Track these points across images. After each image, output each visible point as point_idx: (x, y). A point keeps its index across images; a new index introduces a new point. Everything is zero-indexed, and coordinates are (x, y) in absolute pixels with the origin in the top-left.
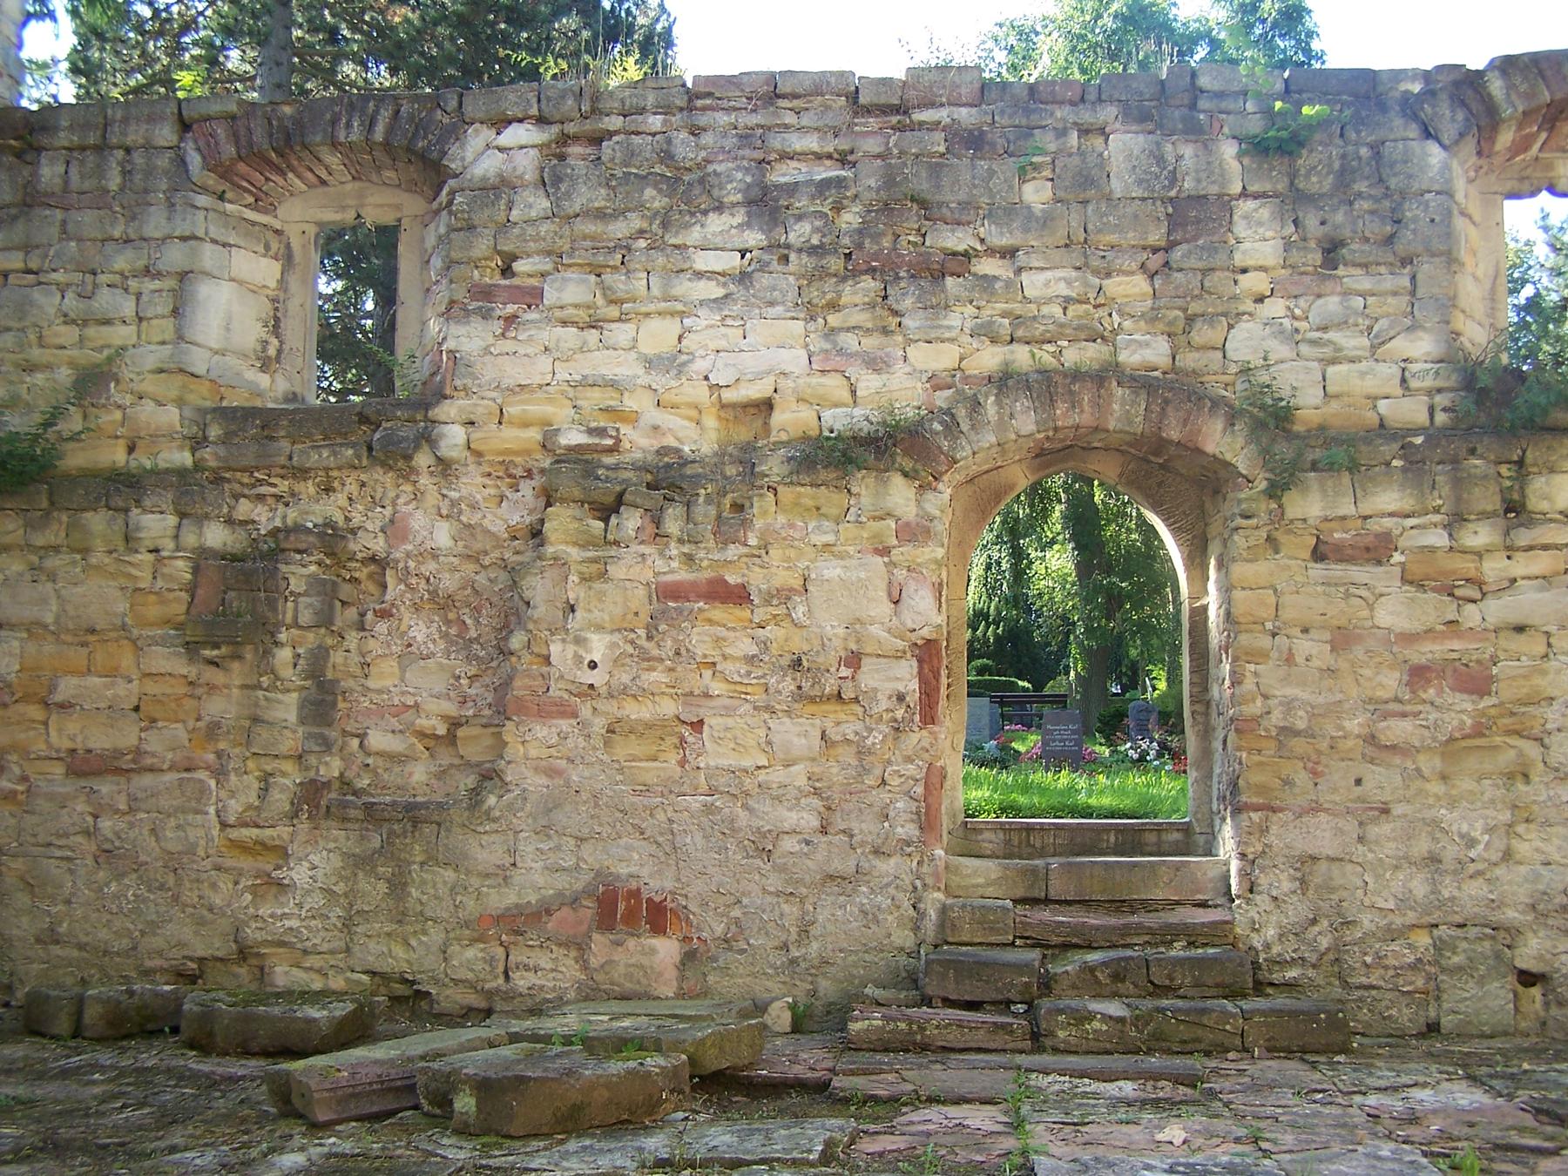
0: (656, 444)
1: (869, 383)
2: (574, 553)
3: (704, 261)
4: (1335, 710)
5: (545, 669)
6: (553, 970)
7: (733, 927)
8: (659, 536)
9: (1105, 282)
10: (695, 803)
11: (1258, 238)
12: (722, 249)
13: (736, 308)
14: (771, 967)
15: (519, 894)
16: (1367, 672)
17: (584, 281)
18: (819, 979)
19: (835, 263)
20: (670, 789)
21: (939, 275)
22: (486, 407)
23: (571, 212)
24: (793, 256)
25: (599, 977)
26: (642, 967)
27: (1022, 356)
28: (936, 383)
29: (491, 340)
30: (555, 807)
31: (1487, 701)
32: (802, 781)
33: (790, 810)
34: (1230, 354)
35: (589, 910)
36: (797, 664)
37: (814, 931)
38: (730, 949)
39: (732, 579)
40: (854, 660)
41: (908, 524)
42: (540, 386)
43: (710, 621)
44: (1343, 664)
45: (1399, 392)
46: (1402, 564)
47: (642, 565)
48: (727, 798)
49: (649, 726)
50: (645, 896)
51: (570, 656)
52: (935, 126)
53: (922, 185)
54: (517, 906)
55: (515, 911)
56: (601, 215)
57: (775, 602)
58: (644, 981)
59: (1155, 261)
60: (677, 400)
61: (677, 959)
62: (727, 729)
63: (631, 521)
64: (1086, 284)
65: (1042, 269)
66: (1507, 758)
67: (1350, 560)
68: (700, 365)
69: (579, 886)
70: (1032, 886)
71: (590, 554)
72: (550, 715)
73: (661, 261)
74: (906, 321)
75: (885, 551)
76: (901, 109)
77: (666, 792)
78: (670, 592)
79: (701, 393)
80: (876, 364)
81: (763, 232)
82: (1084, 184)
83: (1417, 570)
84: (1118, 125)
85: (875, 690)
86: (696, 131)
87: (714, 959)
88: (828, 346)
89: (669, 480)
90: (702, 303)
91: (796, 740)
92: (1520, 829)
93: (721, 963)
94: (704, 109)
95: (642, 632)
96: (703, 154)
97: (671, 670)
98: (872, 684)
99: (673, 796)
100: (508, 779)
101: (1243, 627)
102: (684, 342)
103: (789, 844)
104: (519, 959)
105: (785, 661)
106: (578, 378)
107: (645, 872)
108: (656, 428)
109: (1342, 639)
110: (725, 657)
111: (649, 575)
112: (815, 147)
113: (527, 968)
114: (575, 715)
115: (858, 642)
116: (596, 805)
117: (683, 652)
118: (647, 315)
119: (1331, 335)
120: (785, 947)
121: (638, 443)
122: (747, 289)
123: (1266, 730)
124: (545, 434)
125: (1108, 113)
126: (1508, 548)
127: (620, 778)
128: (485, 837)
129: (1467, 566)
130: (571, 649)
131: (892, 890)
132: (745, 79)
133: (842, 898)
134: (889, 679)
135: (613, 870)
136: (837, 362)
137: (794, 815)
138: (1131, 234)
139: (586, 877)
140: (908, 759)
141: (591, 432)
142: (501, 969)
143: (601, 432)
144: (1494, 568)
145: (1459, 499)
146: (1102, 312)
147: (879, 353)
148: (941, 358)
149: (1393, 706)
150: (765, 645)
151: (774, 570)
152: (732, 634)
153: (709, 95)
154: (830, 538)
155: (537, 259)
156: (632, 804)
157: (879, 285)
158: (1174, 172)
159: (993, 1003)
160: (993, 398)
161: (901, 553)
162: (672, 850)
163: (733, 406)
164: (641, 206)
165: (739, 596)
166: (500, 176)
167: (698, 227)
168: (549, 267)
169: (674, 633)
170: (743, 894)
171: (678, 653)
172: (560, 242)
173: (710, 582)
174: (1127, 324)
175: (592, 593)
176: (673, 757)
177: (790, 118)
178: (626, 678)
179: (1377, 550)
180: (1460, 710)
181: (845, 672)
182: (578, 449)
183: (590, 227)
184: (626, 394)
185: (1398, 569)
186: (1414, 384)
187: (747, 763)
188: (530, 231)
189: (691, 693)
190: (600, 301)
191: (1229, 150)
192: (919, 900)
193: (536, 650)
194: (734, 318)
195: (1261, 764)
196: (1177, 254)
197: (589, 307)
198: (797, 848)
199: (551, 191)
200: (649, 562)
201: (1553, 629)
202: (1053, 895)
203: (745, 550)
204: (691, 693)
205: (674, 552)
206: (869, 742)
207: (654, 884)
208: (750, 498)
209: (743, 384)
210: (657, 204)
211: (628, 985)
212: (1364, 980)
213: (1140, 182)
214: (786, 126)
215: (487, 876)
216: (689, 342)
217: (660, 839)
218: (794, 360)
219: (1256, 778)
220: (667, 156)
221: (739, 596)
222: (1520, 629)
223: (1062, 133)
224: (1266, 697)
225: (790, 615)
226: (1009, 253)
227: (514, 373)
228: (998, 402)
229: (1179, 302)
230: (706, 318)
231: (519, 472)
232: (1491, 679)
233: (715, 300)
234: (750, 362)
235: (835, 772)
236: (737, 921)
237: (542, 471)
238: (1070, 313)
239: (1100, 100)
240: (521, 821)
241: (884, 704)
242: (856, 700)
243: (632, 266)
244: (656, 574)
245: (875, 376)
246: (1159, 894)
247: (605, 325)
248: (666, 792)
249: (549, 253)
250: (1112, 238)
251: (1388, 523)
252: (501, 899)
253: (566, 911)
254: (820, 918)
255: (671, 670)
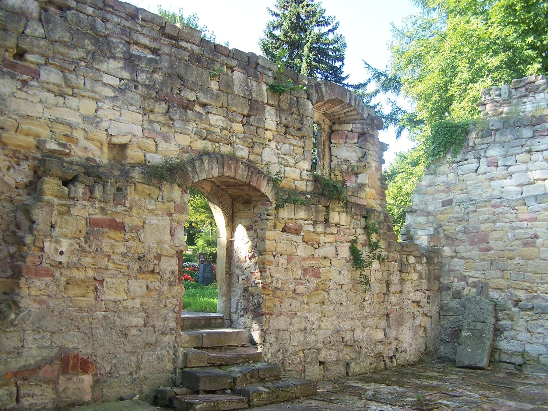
0: (85, 156)
1: (163, 145)
2: (56, 201)
3: (107, 79)
4: (287, 282)
5: (40, 254)
6: (41, 395)
7: (113, 368)
8: (92, 198)
9: (233, 124)
10: (100, 315)
11: (271, 119)
12: (114, 76)
13: (119, 103)
14: (126, 383)
15: (26, 361)
16: (295, 270)
17: (58, 73)
18: (143, 386)
19: (154, 94)
20: (91, 310)
21: (186, 108)
22: (12, 123)
23: (54, 39)
24: (140, 87)
25: (62, 396)
26: (79, 389)
27: (210, 146)
28: (184, 150)
29: (15, 90)
30: (43, 318)
31: (319, 280)
32: (139, 306)
33: (134, 317)
34: (263, 158)
35: (57, 365)
36: (139, 258)
37: (142, 366)
38: (111, 377)
39: (119, 220)
40: (159, 257)
41: (178, 205)
42: (37, 118)
43: (109, 237)
44: (289, 267)
45: (300, 179)
46: (303, 236)
47: (84, 210)
48: (112, 313)
49: (84, 282)
50: (80, 357)
51: (53, 248)
52: (186, 49)
53: (182, 71)
54: (24, 366)
55: (23, 369)
56: (65, 44)
57: (133, 231)
58: (80, 395)
59: (245, 120)
60: (94, 137)
61: (92, 383)
62: (113, 283)
63: (80, 189)
64: (228, 124)
65: (215, 114)
66: (320, 298)
67: (291, 233)
68: (105, 125)
69: (52, 354)
70: (198, 343)
71: (63, 202)
72: (42, 275)
73: (91, 74)
74: (175, 124)
75: (170, 215)
76: (176, 39)
77: (89, 310)
78: (92, 223)
79: (103, 136)
80: (166, 139)
81: (130, 74)
82: (227, 86)
83: (306, 238)
84: (237, 68)
85: (165, 270)
86: (105, 20)
87: (105, 382)
88: (150, 127)
89: (92, 173)
90: (106, 97)
91: (137, 288)
92: (322, 319)
93: (108, 383)
94: (109, 12)
95: (83, 240)
96: (107, 32)
97: (94, 257)
98: (165, 267)
99: (92, 312)
100: (21, 305)
101: (267, 253)
102: (98, 113)
103: (134, 331)
104: (25, 391)
105: (136, 256)
106: (54, 118)
107: (80, 346)
108: (86, 148)
109: (290, 258)
110: (113, 253)
111: (86, 215)
112: (148, 43)
113: (29, 395)
114: (53, 276)
115: (161, 250)
116: (61, 317)
117: (99, 250)
118: (84, 97)
119: (287, 157)
120: (131, 374)
121: (78, 153)
122: (123, 96)
123: (272, 288)
124: (39, 141)
125: (235, 63)
126: (325, 233)
127: (71, 304)
128: (10, 334)
129: (315, 237)
130: (53, 245)
131: (168, 348)
132: (127, 6)
133: (151, 352)
134: (170, 265)
135: (66, 346)
136: (153, 135)
137: (136, 320)
138: (240, 109)
139: (56, 350)
140: (174, 297)
141: (60, 144)
142: (15, 396)
143: (64, 146)
144: (322, 239)
145: (316, 216)
146: (230, 135)
147: (167, 135)
148: (185, 141)
149: (299, 281)
150: (129, 249)
151: (133, 217)
152: (117, 243)
153: (112, 7)
154: (153, 207)
155: (37, 56)
156: (76, 316)
157: (167, 107)
158: (251, 90)
159: (220, 390)
160: (207, 161)
161: (176, 216)
162: (90, 336)
163: (114, 145)
164: (83, 47)
165: (121, 227)
166: (21, 9)
167: (106, 64)
168: (43, 62)
169: (96, 241)
170: (118, 353)
171: (97, 250)
172: (49, 52)
173: (110, 220)
174: (238, 141)
175: (63, 220)
176: (92, 295)
177: (139, 29)
178: (75, 260)
179: (297, 231)
180: (313, 282)
181: (156, 262)
182: (53, 151)
183: (63, 49)
184: (74, 130)
185: (302, 237)
186: (303, 177)
187: (120, 298)
188: (35, 42)
189: (101, 268)
190: (63, 85)
191: (264, 87)
192: (176, 351)
193: (38, 244)
194: (117, 107)
195: (269, 299)
196: (252, 119)
197: (59, 86)
198: (136, 333)
199: (45, 26)
200: (87, 209)
201: (331, 258)
202: (204, 346)
203: (124, 208)
204: (101, 268)
205: (97, 206)
206: (162, 290)
207: (84, 351)
208: (126, 186)
209: (120, 136)
210: (89, 48)
211: (74, 398)
212: (289, 368)
213: (243, 91)
214: (137, 30)
215: (9, 353)
216: (100, 113)
217: (87, 331)
218: (137, 130)
219: (268, 304)
220: (93, 28)
221: (121, 227)
222: (325, 258)
223: (222, 65)
224: (272, 277)
225: (138, 237)
226: (204, 105)
227: (25, 108)
228: (208, 163)
229: (251, 137)
230: (107, 105)
231: (21, 156)
232: (320, 273)
233: (111, 97)
234: (124, 128)
235: (150, 302)
236: (115, 365)
237: (35, 158)
238: (223, 133)
239: (233, 57)
240: (27, 325)
241: (168, 275)
242: (159, 273)
243: (78, 73)
244: (89, 214)
245: (165, 143)
246: (232, 343)
247: (67, 97)
248: (89, 310)
249: (43, 56)
250: (234, 109)
251: (302, 222)
252: (16, 364)
253: (47, 367)
254: (144, 361)
255: (94, 257)
